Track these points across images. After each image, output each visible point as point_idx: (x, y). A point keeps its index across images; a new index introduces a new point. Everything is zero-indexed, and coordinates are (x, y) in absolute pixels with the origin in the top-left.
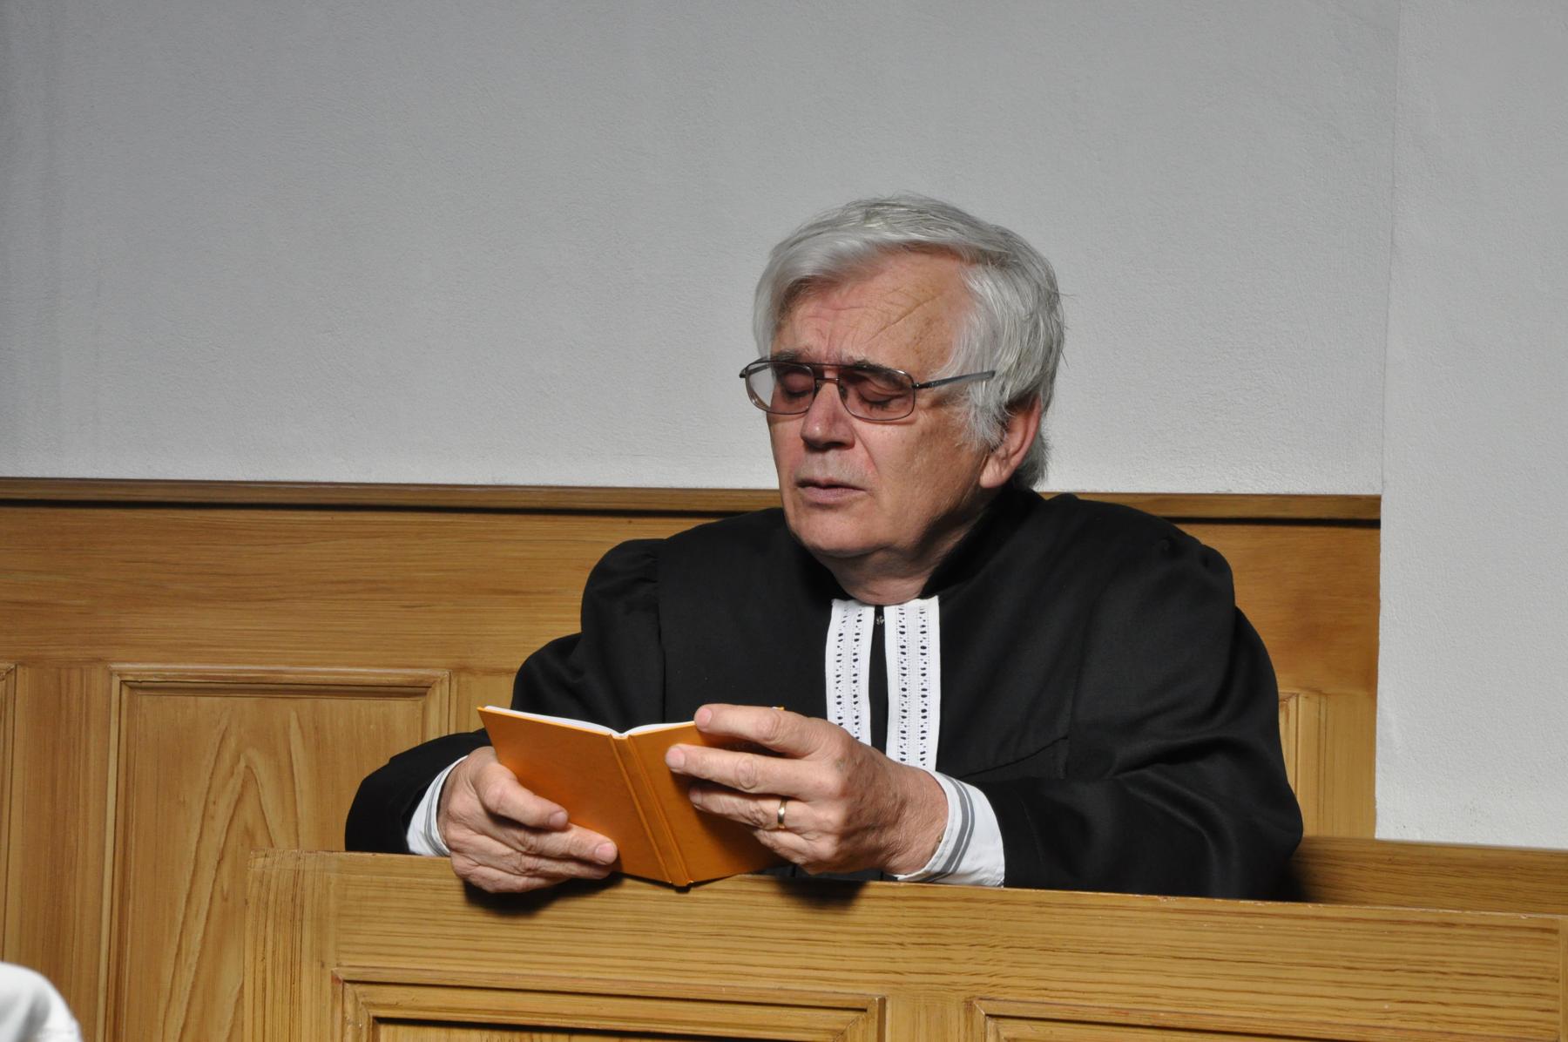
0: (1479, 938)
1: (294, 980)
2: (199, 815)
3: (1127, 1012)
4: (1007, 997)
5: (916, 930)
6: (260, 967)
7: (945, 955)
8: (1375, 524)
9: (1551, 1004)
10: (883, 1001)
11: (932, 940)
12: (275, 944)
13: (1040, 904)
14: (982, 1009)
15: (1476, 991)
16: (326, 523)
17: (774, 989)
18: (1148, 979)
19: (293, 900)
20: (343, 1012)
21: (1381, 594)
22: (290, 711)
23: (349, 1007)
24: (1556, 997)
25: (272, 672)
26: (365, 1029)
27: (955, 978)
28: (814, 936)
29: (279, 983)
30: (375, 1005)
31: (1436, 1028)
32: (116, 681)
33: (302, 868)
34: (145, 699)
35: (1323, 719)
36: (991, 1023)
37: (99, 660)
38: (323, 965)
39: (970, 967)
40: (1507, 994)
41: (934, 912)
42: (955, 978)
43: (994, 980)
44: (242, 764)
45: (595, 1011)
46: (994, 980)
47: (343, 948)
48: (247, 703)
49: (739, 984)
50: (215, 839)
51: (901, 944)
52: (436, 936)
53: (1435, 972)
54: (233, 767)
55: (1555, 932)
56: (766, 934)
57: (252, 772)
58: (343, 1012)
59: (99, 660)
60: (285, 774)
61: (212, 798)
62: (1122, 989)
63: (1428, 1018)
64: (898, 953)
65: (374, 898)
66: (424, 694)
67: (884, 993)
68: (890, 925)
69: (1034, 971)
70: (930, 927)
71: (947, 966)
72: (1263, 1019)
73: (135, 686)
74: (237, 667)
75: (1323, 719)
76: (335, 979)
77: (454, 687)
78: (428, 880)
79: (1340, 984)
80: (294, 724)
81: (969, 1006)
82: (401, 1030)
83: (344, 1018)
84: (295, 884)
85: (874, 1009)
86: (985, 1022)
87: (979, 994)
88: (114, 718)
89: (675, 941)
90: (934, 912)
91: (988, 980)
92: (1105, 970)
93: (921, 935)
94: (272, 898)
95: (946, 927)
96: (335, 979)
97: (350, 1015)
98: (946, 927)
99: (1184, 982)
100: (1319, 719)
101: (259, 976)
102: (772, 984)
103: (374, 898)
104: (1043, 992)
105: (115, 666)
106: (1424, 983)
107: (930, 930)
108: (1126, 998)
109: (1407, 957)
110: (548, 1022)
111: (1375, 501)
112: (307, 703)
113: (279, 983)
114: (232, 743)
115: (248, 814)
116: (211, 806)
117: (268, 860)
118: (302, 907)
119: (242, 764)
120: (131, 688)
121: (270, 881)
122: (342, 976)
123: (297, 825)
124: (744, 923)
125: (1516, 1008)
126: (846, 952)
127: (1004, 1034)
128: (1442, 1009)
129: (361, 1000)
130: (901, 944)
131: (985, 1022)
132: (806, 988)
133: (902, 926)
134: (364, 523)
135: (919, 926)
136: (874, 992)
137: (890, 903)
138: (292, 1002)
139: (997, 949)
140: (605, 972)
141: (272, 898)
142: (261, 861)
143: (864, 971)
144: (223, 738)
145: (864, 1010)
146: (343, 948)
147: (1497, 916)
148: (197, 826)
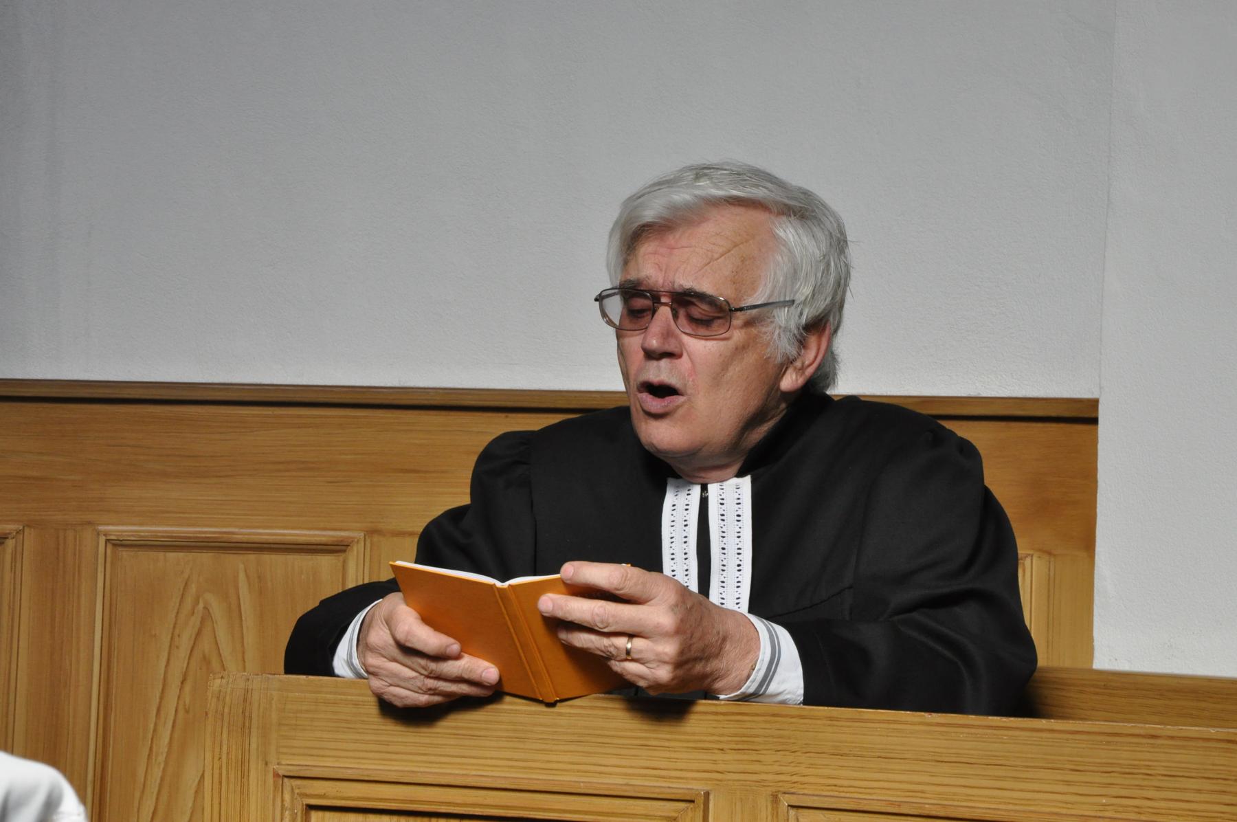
1: (244, 775)
2: (166, 645)
3: (899, 804)
6: (217, 766)
8: (1094, 421)
10: (707, 794)
11: (746, 747)
14: (785, 801)
15: (1175, 789)
18: (915, 778)
20: (283, 801)
22: (239, 564)
23: (287, 797)
32: (102, 539)
33: (250, 687)
34: (125, 554)
35: (1052, 574)
36: (792, 812)
37: (89, 523)
38: (266, 764)
39: (776, 768)
40: (1199, 791)
41: (748, 725)
43: (795, 778)
44: (201, 606)
45: (480, 801)
48: (206, 558)
51: (722, 750)
52: (356, 741)
56: (615, 741)
57: (209, 613)
58: (283, 801)
59: (89, 523)
60: (235, 614)
61: (177, 631)
64: (719, 756)
65: (307, 711)
66: (345, 551)
67: (707, 788)
71: (757, 767)
73: (118, 544)
75: (1052, 574)
76: (276, 775)
79: (1068, 783)
80: (242, 576)
81: (775, 798)
83: (283, 805)
84: (245, 700)
85: (700, 801)
86: (788, 812)
88: (100, 569)
90: (748, 725)
92: (881, 771)
93: (737, 743)
94: (226, 710)
95: (757, 736)
96: (276, 775)
97: (287, 803)
98: (757, 736)
99: (946, 781)
100: (1049, 575)
101: (216, 772)
103: (307, 711)
109: (1121, 762)
110: (443, 809)
111: (1094, 404)
112: (252, 557)
114: (193, 589)
115: (206, 645)
116: (177, 639)
117: (224, 681)
118: (250, 717)
119: (201, 606)
120: (114, 545)
122: (281, 773)
123: (243, 653)
129: (297, 791)
130: (722, 750)
131: (788, 810)
135: (736, 735)
136: (700, 787)
138: (242, 793)
141: (226, 710)
142: (218, 681)
143: (692, 771)
145: (692, 801)
148: (166, 654)
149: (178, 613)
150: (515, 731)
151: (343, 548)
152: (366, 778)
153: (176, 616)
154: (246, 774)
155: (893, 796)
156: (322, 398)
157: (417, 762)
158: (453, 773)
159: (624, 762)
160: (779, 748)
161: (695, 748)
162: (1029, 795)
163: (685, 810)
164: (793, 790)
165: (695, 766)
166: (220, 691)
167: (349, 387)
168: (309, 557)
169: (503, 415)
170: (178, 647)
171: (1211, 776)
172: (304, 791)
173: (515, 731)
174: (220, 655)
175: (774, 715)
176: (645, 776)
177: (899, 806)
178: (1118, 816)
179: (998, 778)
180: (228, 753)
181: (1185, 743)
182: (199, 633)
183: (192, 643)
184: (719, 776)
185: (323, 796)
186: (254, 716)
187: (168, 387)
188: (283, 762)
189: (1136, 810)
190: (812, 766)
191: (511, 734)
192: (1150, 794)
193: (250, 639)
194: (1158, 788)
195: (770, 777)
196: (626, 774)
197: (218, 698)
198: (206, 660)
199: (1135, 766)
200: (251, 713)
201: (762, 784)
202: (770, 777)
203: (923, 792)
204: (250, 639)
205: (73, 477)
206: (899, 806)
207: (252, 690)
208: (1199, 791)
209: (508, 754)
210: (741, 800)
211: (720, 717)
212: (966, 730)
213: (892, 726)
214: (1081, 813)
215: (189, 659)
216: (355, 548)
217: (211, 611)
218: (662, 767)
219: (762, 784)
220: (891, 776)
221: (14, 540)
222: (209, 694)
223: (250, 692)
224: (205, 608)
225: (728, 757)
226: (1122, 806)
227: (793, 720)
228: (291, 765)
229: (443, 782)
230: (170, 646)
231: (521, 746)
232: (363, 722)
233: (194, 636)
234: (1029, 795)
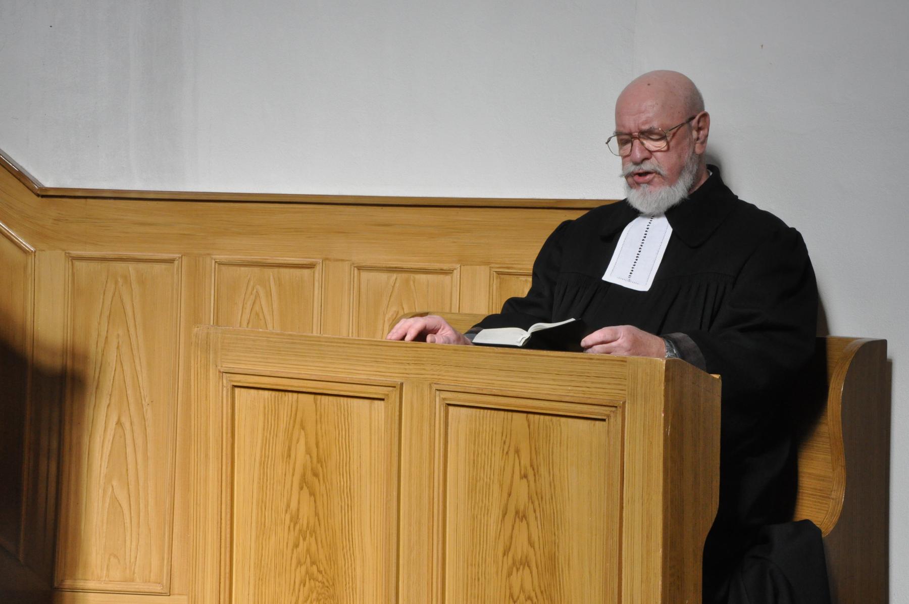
0: (601, 364)
1: (207, 371)
2: (241, 308)
3: (482, 389)
4: (444, 383)
5: (413, 359)
6: (196, 366)
7: (424, 368)
9: (623, 388)
10: (402, 384)
14: (435, 387)
15: (600, 383)
16: (281, 208)
17: (365, 379)
18: (491, 377)
20: (222, 383)
22: (270, 273)
23: (225, 381)
24: (625, 385)
25: (263, 259)
26: (229, 389)
27: (426, 376)
29: (202, 372)
30: (232, 381)
31: (586, 396)
32: (213, 262)
34: (223, 268)
36: (438, 392)
37: (209, 254)
38: (217, 366)
39: (432, 372)
41: (419, 352)
42: (426, 376)
43: (440, 377)
44: (255, 290)
45: (305, 385)
46: (440, 377)
47: (223, 360)
48: (256, 270)
49: (354, 377)
50: (246, 317)
51: (408, 364)
52: (253, 357)
53: (585, 376)
55: (626, 362)
58: (222, 383)
59: (209, 254)
60: (269, 294)
61: (245, 302)
62: (481, 381)
64: (407, 367)
65: (233, 343)
66: (314, 268)
67: (402, 381)
68: (404, 357)
69: (452, 374)
72: (529, 393)
73: (221, 264)
74: (253, 257)
76: (220, 372)
77: (324, 265)
78: (251, 337)
79: (554, 380)
80: (271, 277)
81: (431, 387)
82: (243, 390)
83: (223, 385)
84: (207, 338)
86: (435, 392)
87: (434, 382)
88: (213, 274)
89: (332, 361)
90: (419, 352)
91: (437, 377)
92: (476, 374)
93: (415, 360)
94: (199, 342)
96: (220, 372)
97: (225, 384)
98: (424, 358)
101: (196, 369)
102: (365, 377)
103: (233, 343)
106: (582, 380)
109: (577, 370)
110: (290, 389)
112: (276, 270)
113: (202, 372)
114: (252, 283)
115: (257, 308)
116: (245, 305)
117: (199, 329)
118: (210, 346)
119: (255, 290)
120: (219, 264)
122: (222, 371)
123: (273, 312)
124: (356, 355)
125: (613, 389)
126: (390, 366)
127: (442, 396)
128: (588, 389)
129: (228, 379)
130: (408, 364)
131: (435, 392)
132: (376, 378)
133: (409, 357)
134: (295, 208)
135: (415, 357)
136: (399, 381)
137: (405, 349)
138: (206, 379)
139: (441, 366)
142: (196, 329)
143: (396, 373)
145: (395, 387)
146: (223, 360)
150: (320, 354)
152: (257, 374)
153: (245, 295)
155: (480, 385)
156: (288, 200)
158: (294, 372)
159: (368, 369)
160: (433, 363)
161: (396, 363)
162: (539, 386)
163: (392, 391)
164: (438, 382)
165: (397, 371)
167: (238, 194)
168: (299, 270)
169: (381, 208)
170: (246, 309)
171: (614, 377)
172: (231, 379)
173: (320, 354)
175: (431, 348)
176: (376, 375)
177: (482, 390)
178: (575, 395)
179: (525, 378)
180: (200, 361)
181: (605, 362)
182: (254, 303)
184: (407, 376)
185: (239, 382)
186: (211, 345)
187: (215, 195)
188: (224, 366)
190: (448, 371)
191: (319, 355)
192: (589, 385)
193: (275, 306)
194: (592, 382)
196: (367, 374)
197: (196, 337)
198: (257, 314)
199: (584, 373)
200: (210, 343)
203: (493, 384)
204: (275, 306)
206: (482, 390)
210: (417, 386)
211: (408, 349)
212: (512, 356)
213: (482, 354)
214: (559, 393)
216: (318, 268)
220: (481, 377)
222: (192, 335)
224: (257, 292)
225: (411, 367)
226: (576, 390)
228: (227, 367)
229: (290, 376)
231: (323, 361)
232: (256, 349)
233: (252, 304)
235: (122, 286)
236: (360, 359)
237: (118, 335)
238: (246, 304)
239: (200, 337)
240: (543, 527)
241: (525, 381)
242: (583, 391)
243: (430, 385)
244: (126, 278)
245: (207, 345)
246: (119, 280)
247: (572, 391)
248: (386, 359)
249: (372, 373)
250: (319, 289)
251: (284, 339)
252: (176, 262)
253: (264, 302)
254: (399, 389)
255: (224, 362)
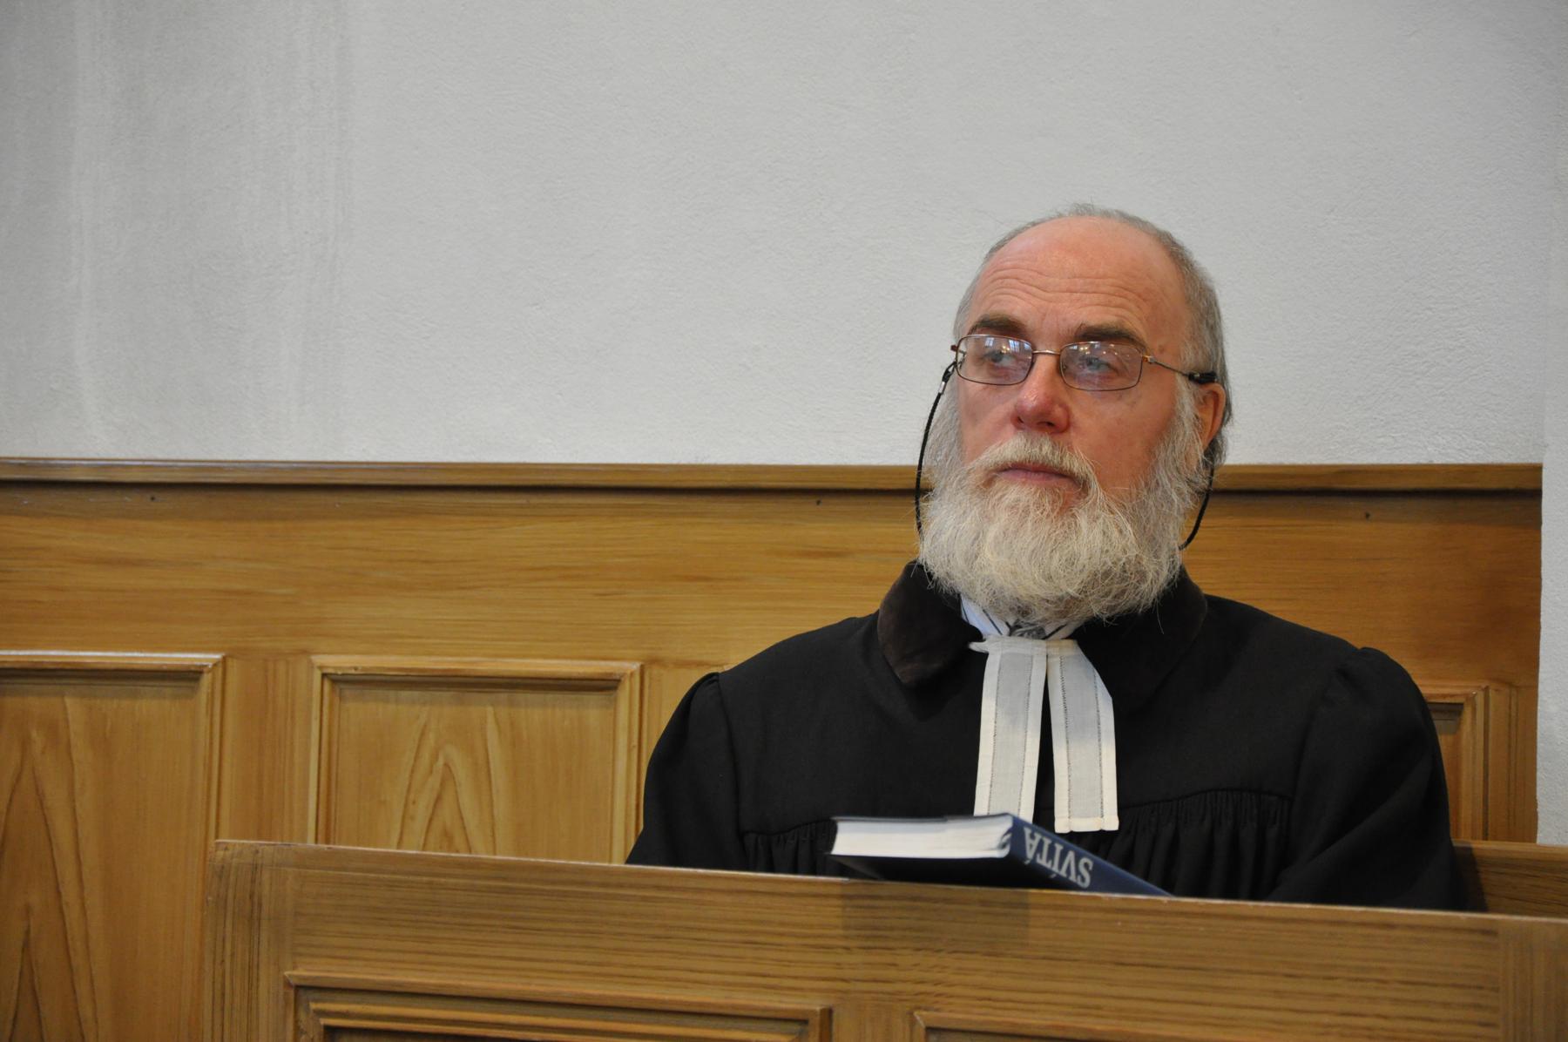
2: (398, 816)
5: (863, 933)
8: (1536, 494)
11: (877, 944)
12: (233, 946)
13: (983, 903)
18: (1089, 987)
19: (251, 896)
21: (1542, 571)
22: (487, 713)
27: (898, 987)
28: (761, 939)
32: (317, 675)
33: (260, 862)
35: (1513, 714)
40: (1446, 1005)
43: (940, 989)
44: (441, 762)
46: (940, 989)
54: (431, 767)
56: (713, 936)
57: (451, 771)
60: (482, 771)
61: (412, 797)
62: (1066, 999)
63: (1367, 1033)
64: (845, 958)
70: (876, 928)
71: (892, 973)
73: (337, 681)
75: (1513, 714)
79: (1278, 994)
84: (253, 881)
85: (815, 1021)
93: (868, 938)
94: (231, 893)
95: (892, 929)
98: (892, 929)
99: (1126, 991)
100: (1510, 715)
104: (987, 1002)
105: (319, 660)
107: (875, 933)
108: (1070, 1010)
111: (1536, 470)
114: (431, 739)
115: (446, 814)
119: (441, 762)
121: (229, 876)
126: (790, 956)
136: (815, 1004)
140: (1449, 1021)
141: (231, 893)
144: (423, 734)
147: (1057, 894)
148: (398, 826)
149: (412, 771)
151: (610, 684)
154: (255, 983)
157: (466, 966)
162: (1232, 1012)
166: (223, 867)
174: (464, 828)
183: (430, 810)
189: (1367, 1033)
195: (909, 987)
197: (220, 877)
201: (898, 997)
202: (909, 987)
203: (1098, 1008)
204: (502, 806)
205: (284, 591)
207: (262, 867)
208: (1446, 1005)
209: (512, 952)
212: (1151, 918)
215: (427, 832)
217: (453, 769)
218: (771, 973)
219: (898, 997)
221: (210, 675)
223: (259, 870)
224: (446, 765)
227: (937, 905)
230: (404, 817)
233: (432, 804)
234: (1232, 1012)
235: (43, 753)
236: (704, 935)
237: (28, 909)
238: (414, 803)
239: (232, 878)
240: (661, 973)
241: (1195, 996)
242: (1369, 1029)
243: (911, 1014)
244: (55, 731)
245: (252, 904)
246: (34, 734)
247: (1335, 1030)
248: (781, 935)
249: (738, 979)
250: (629, 751)
251: (479, 878)
252: (206, 679)
253: (467, 801)
254: (818, 1029)
255: (301, 955)
